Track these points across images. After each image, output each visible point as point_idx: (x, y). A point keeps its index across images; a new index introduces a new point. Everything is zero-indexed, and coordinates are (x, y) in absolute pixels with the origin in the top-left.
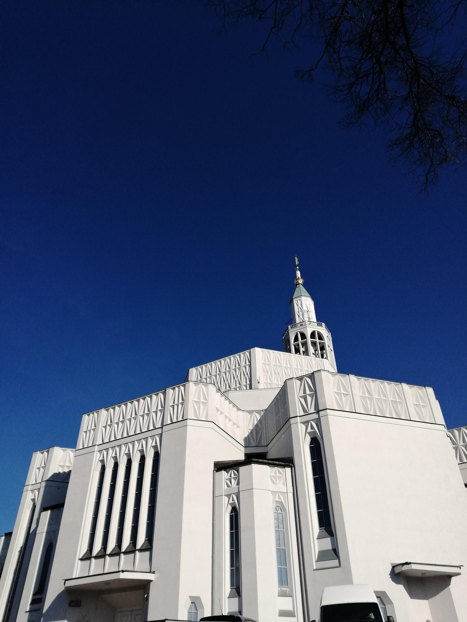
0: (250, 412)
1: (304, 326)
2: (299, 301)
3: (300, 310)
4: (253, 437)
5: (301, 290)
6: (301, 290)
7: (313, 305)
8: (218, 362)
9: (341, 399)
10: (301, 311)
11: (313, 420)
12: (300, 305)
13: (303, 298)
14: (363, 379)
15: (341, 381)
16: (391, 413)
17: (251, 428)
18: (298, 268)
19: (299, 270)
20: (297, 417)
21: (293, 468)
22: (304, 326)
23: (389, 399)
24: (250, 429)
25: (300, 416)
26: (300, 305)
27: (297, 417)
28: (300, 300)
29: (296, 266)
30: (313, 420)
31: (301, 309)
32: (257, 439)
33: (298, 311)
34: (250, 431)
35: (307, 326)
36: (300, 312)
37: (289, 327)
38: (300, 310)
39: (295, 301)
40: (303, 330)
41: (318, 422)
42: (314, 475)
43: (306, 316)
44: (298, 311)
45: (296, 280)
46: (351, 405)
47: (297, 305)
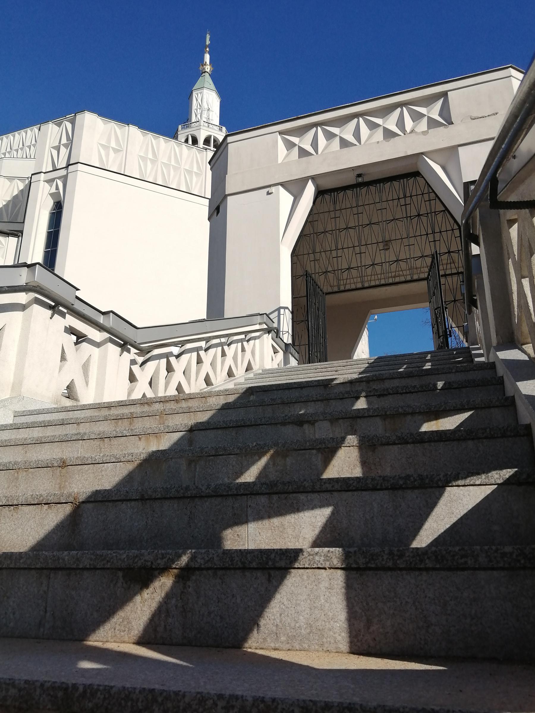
0: (11, 179)
1: (198, 128)
2: (199, 94)
3: (199, 107)
4: (7, 211)
5: (207, 80)
6: (207, 80)
7: (218, 104)
8: (23, 132)
9: (107, 155)
10: (200, 109)
11: (59, 178)
12: (200, 101)
13: (205, 91)
14: (150, 136)
15: (115, 132)
16: (179, 184)
17: (9, 199)
18: (208, 49)
19: (209, 53)
20: (41, 172)
21: (21, 238)
22: (198, 128)
23: (182, 167)
24: (5, 201)
25: (44, 173)
26: (200, 101)
27: (41, 172)
28: (201, 93)
29: (206, 47)
30: (59, 178)
31: (200, 106)
32: (12, 214)
33: (196, 108)
34: (4, 203)
35: (202, 127)
36: (198, 110)
37: (180, 127)
38: (199, 107)
39: (194, 94)
40: (195, 133)
41: (65, 179)
42: (46, 248)
43: (205, 115)
44: (196, 108)
45: (203, 66)
46: (120, 164)
47: (197, 100)
